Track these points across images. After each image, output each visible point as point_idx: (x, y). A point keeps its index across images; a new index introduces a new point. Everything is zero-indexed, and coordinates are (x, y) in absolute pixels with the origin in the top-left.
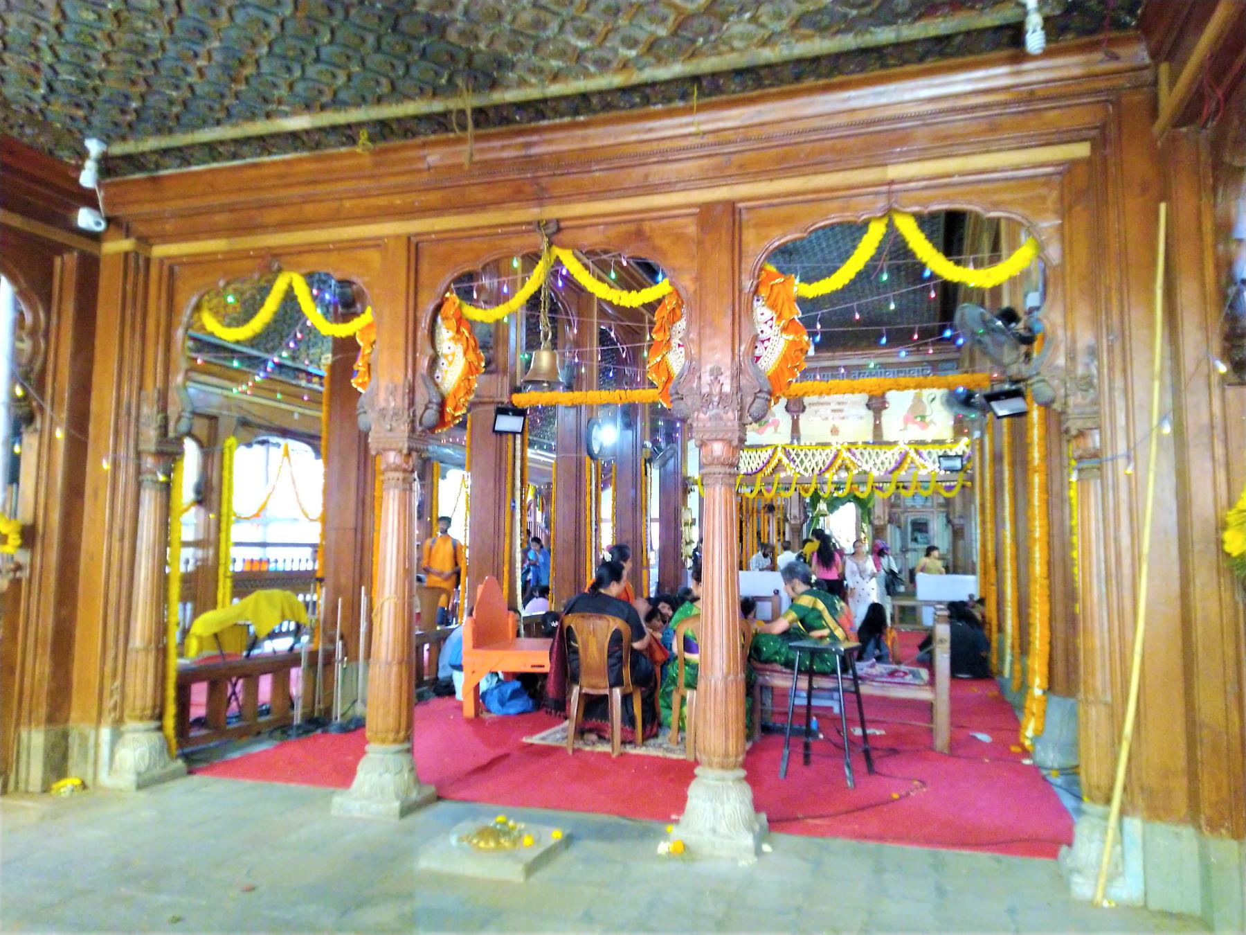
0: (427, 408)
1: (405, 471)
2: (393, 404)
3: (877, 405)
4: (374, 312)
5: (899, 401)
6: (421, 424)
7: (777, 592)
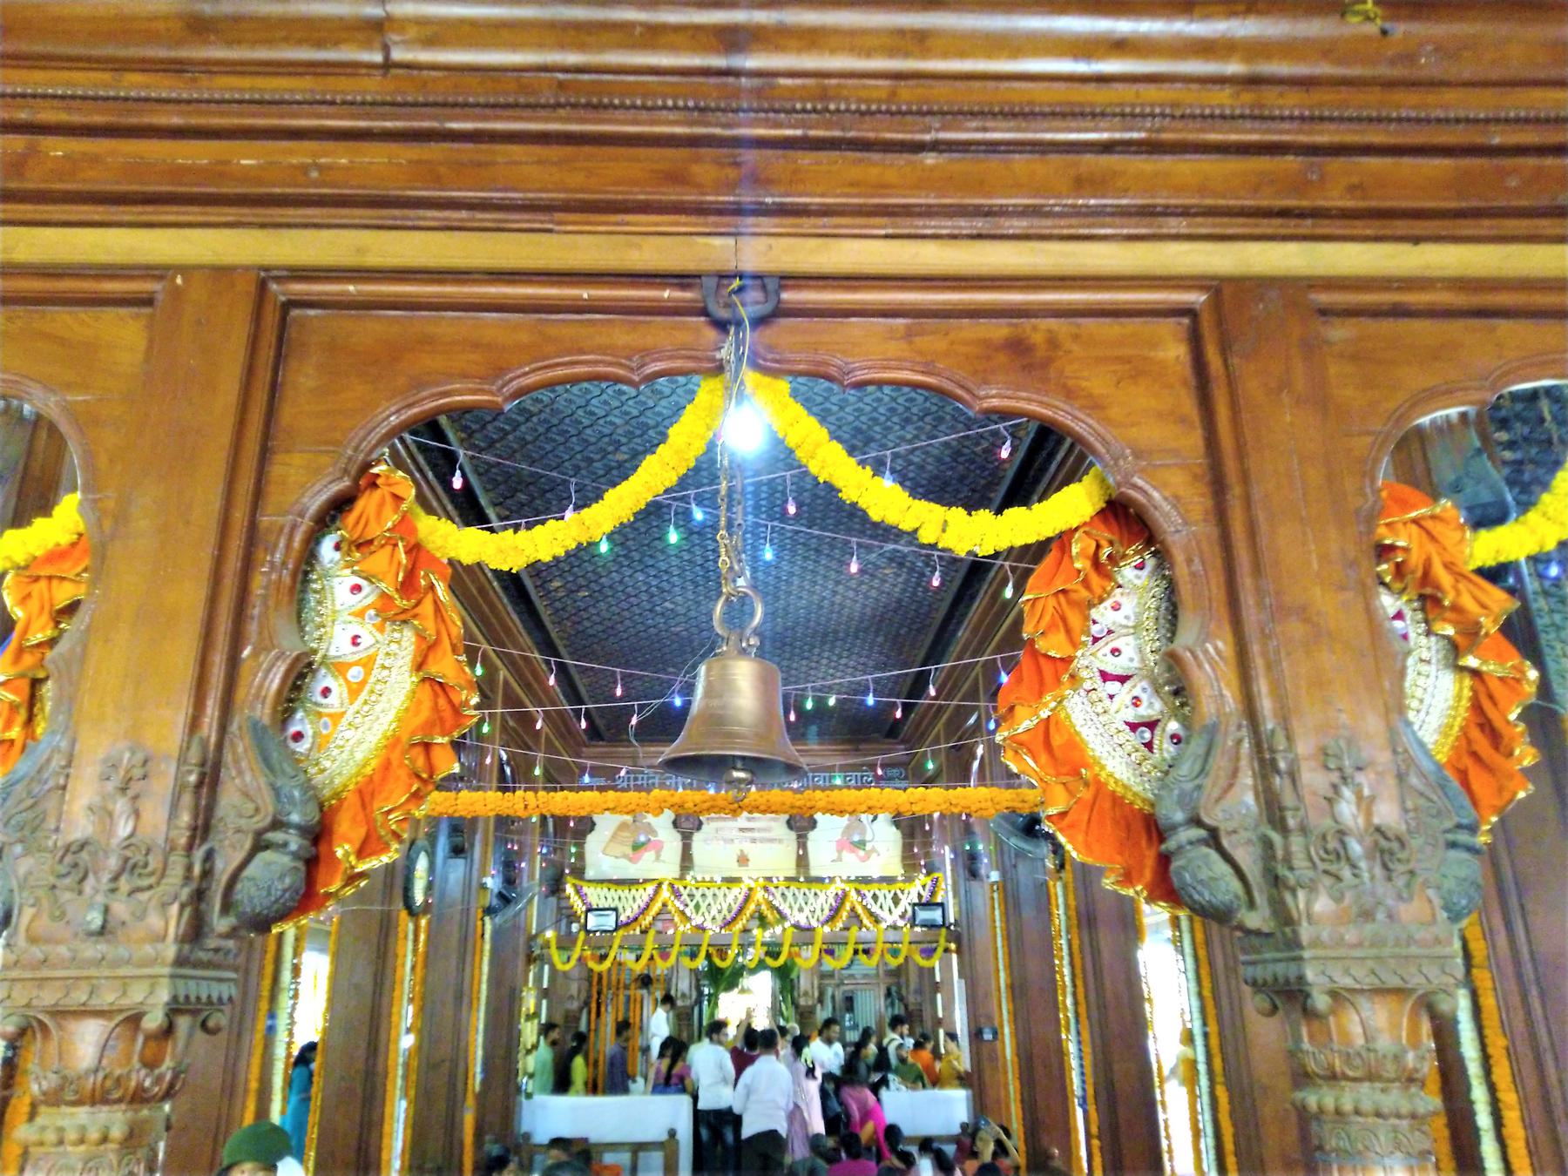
0: (259, 845)
1: (139, 1097)
2: (124, 829)
3: (801, 824)
4: (90, 507)
5: (829, 828)
6: (226, 907)
7: (672, 1134)
